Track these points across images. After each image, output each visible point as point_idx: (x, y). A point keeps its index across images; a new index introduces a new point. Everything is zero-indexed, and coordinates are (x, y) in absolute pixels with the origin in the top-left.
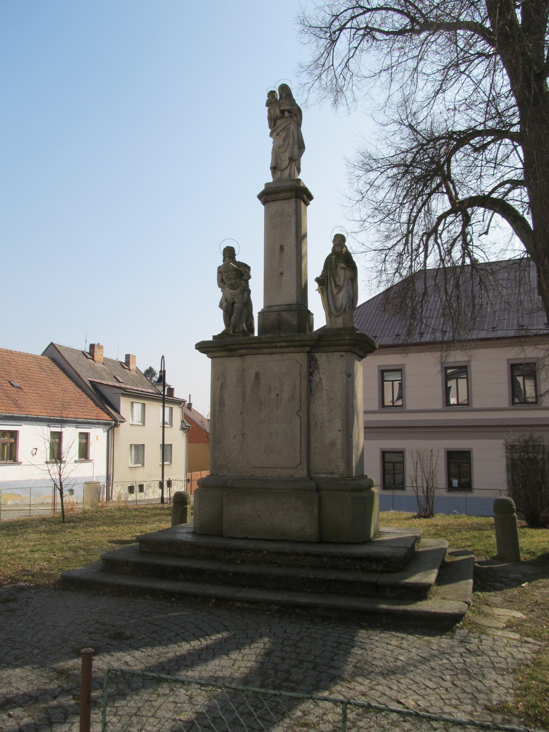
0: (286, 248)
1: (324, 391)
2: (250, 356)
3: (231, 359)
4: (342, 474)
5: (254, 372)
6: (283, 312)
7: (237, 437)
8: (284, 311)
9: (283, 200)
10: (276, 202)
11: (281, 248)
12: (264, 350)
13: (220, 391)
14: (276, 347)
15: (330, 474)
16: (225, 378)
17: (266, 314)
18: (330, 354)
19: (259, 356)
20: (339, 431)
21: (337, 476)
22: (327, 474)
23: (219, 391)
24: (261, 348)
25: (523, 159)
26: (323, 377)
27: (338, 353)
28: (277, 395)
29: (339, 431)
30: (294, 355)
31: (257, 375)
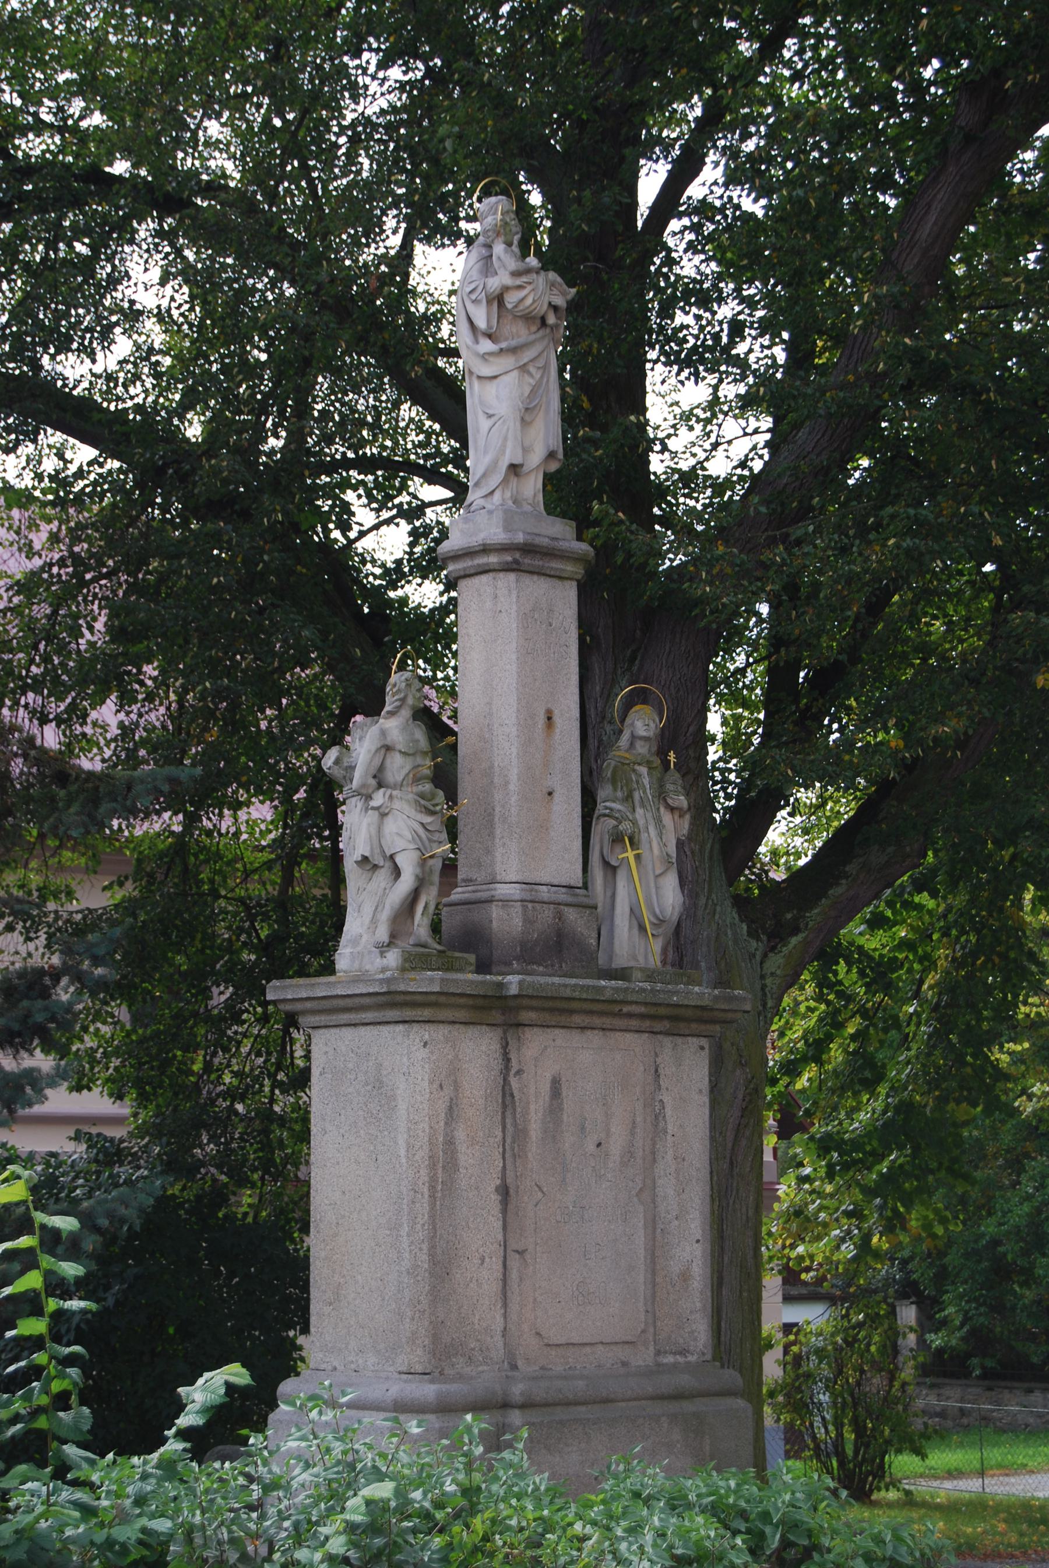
0: (557, 719)
1: (669, 1137)
2: (535, 1029)
3: (472, 1031)
4: (703, 1354)
5: (548, 1076)
6: (566, 909)
7: (487, 1260)
8: (567, 905)
9: (550, 576)
10: (535, 577)
11: (549, 718)
12: (577, 1019)
13: (446, 1123)
14: (620, 1015)
15: (680, 1353)
16: (457, 1086)
17: (530, 905)
18: (679, 1040)
19: (557, 1031)
20: (698, 1241)
21: (692, 1359)
22: (675, 1354)
23: (442, 1124)
24: (572, 1012)
25: (521, 307)
26: (666, 1098)
27: (695, 1039)
28: (599, 1145)
29: (698, 1241)
30: (629, 1036)
31: (556, 1086)
